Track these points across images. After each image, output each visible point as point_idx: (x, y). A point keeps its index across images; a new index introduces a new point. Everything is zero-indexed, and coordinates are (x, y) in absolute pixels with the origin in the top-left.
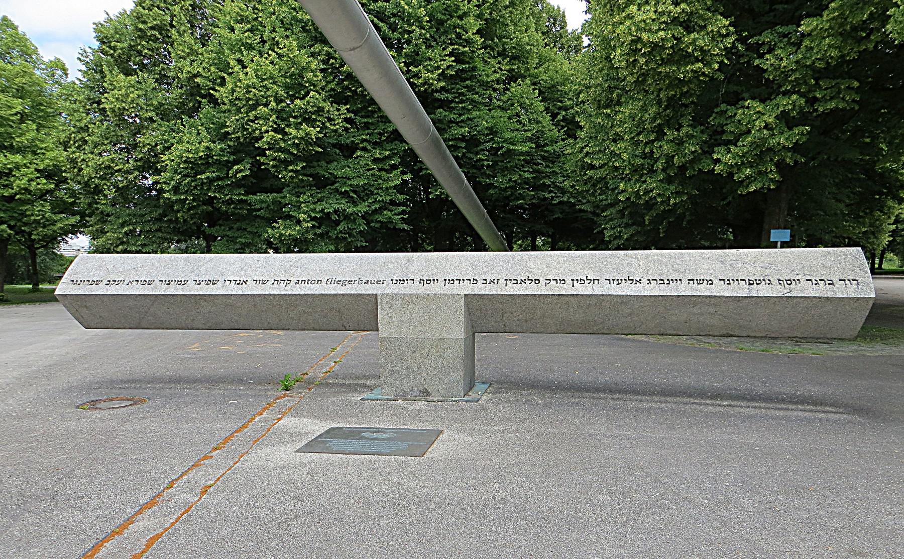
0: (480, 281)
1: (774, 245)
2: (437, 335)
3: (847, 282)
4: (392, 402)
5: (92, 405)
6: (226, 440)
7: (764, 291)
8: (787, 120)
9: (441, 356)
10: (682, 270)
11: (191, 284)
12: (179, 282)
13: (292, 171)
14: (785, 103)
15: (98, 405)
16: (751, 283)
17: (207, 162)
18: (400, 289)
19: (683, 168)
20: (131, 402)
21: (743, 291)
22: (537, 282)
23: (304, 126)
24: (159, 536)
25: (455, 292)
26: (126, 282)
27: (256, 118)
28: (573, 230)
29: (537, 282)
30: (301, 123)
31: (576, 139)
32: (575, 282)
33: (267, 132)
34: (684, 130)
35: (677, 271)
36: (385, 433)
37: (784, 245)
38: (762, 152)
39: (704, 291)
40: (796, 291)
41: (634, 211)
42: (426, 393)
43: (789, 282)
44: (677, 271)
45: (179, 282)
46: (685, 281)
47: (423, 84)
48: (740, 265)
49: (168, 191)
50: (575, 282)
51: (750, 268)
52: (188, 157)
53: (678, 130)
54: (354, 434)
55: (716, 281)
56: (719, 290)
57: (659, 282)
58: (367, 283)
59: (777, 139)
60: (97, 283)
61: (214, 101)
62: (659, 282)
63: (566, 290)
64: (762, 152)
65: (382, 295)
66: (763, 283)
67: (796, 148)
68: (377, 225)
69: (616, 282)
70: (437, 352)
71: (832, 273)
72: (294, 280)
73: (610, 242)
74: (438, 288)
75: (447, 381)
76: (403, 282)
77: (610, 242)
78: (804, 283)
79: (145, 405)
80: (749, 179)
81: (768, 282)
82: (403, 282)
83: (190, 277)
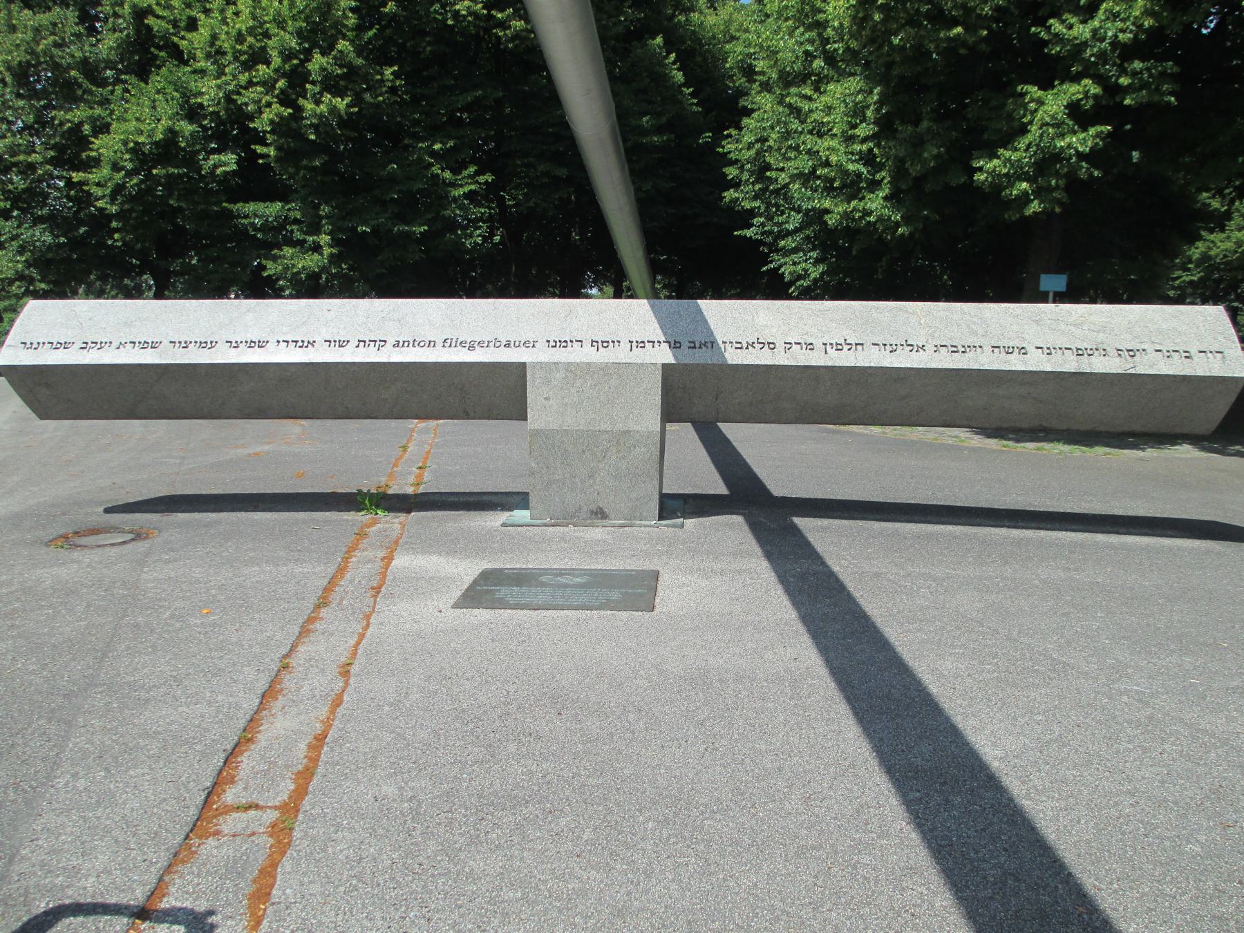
0: (685, 345)
1: (1042, 298)
2: (620, 426)
4: (551, 529)
5: (70, 540)
6: (329, 589)
7: (1099, 365)
8: (1079, 115)
9: (624, 457)
12: (203, 345)
13: (306, 168)
14: (1073, 91)
15: (83, 541)
17: (167, 149)
18: (561, 355)
19: (920, 180)
20: (131, 536)
21: (1070, 364)
22: (772, 346)
23: (327, 97)
24: (321, 739)
25: (648, 360)
26: (116, 344)
27: (250, 84)
29: (772, 346)
30: (321, 93)
31: (740, 129)
32: (828, 347)
33: (269, 105)
34: (925, 124)
35: (975, 333)
36: (574, 575)
37: (1060, 298)
38: (1047, 161)
39: (1015, 363)
41: (825, 238)
42: (600, 514)
43: (1132, 353)
44: (975, 333)
45: (203, 345)
46: (987, 349)
47: (513, 39)
48: (1063, 327)
49: (104, 197)
50: (828, 347)
51: (1078, 332)
52: (137, 143)
53: (916, 123)
54: (521, 578)
55: (1031, 349)
58: (508, 345)
59: (1068, 140)
61: (179, 56)
63: (816, 359)
64: (1047, 161)
67: (1091, 157)
69: (888, 347)
70: (619, 452)
71: (1173, 338)
72: (391, 341)
73: (791, 283)
74: (621, 354)
75: (634, 495)
76: (564, 344)
77: (791, 283)
79: (159, 540)
80: (1024, 199)
82: (564, 344)
83: (222, 336)
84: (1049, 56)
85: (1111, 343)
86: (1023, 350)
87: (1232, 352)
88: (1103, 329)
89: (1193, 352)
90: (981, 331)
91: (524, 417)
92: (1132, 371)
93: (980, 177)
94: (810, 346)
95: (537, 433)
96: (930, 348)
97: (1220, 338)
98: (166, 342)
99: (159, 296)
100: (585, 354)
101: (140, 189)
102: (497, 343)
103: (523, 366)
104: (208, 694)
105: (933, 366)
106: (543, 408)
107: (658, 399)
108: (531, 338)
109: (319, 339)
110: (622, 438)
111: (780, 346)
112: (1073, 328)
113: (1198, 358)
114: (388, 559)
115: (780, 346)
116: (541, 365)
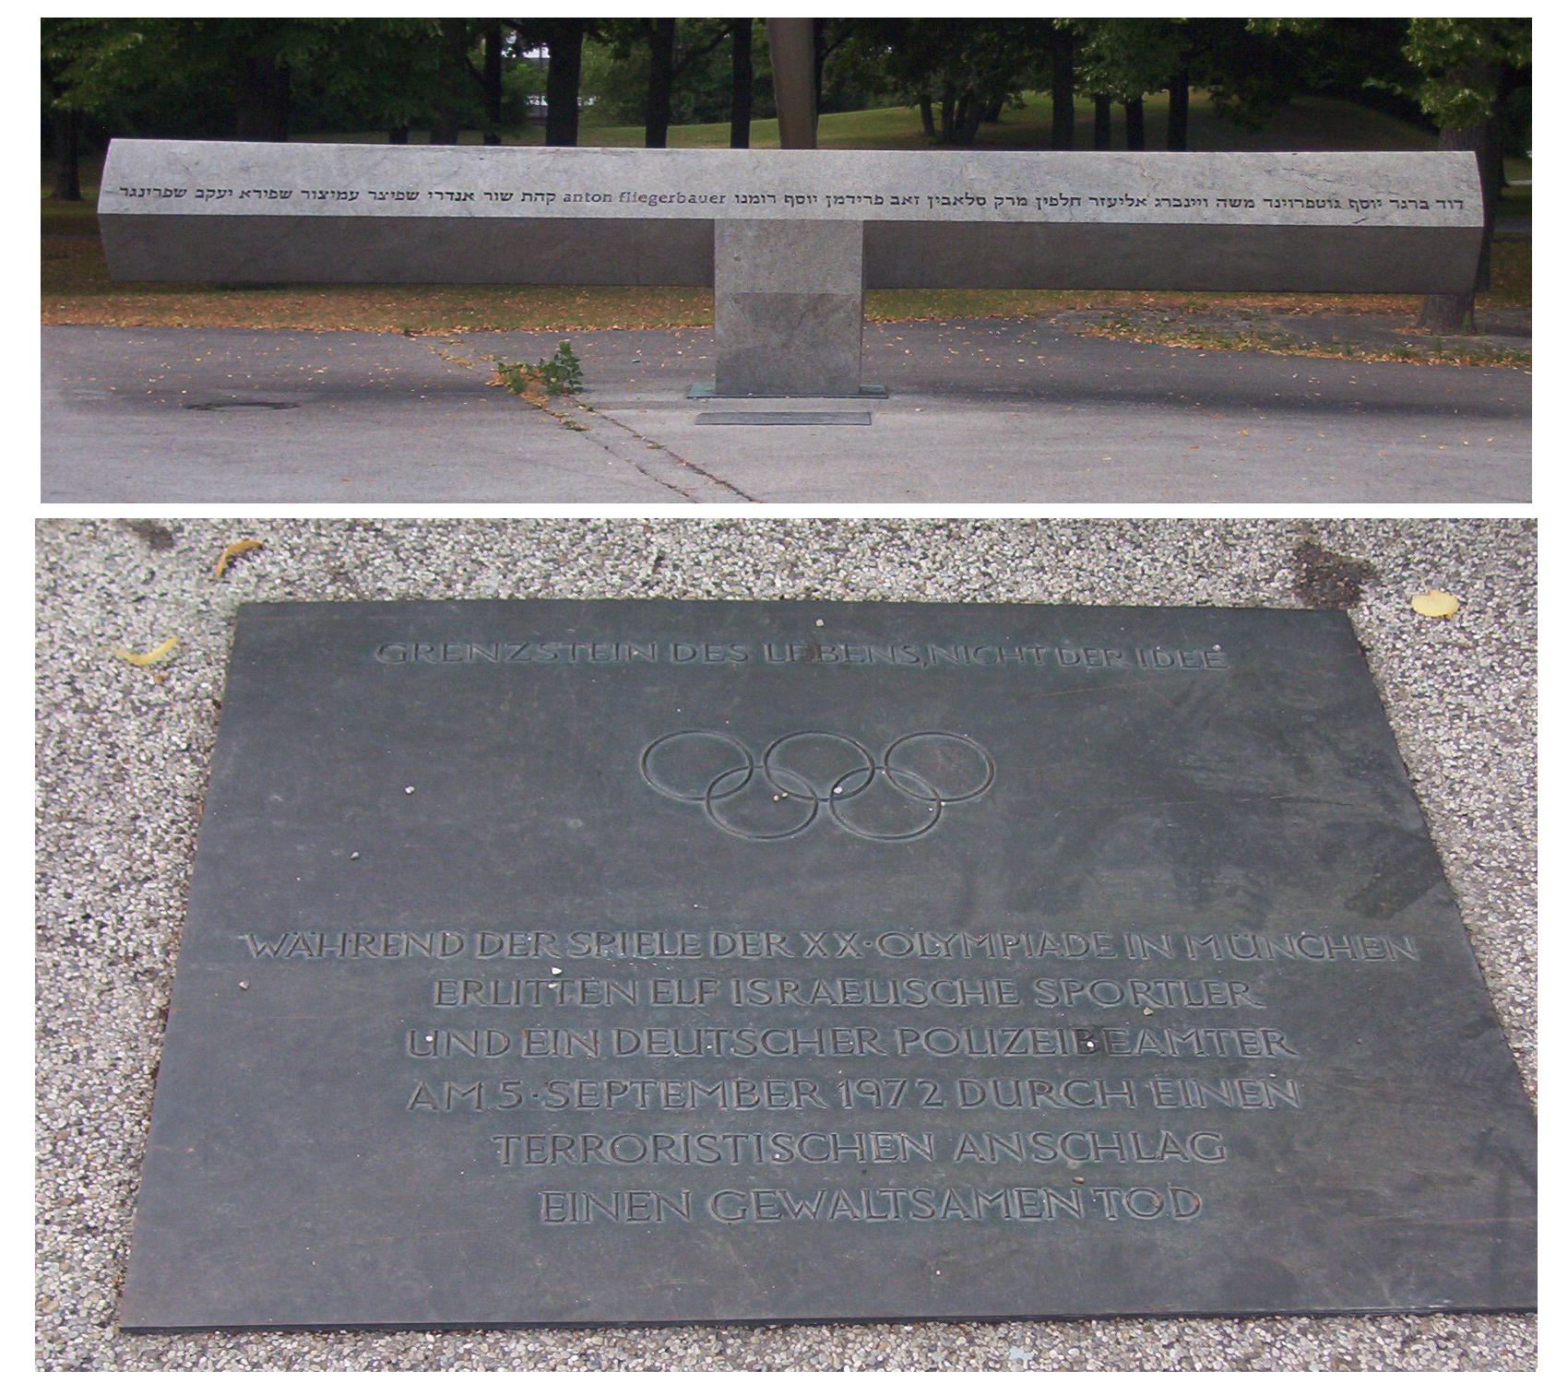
2: (818, 290)
22: (981, 201)
25: (848, 216)
29: (981, 201)
39: (1243, 217)
43: (1366, 204)
44: (1201, 186)
46: (1212, 203)
58: (692, 200)
63: (1030, 215)
76: (755, 199)
84: (1402, 59)
85: (1345, 191)
86: (1250, 203)
88: (1339, 179)
90: (1208, 183)
94: (1023, 201)
96: (1151, 202)
97: (1464, 187)
98: (296, 193)
100: (766, 212)
101: (1467, 43)
102: (681, 198)
105: (1154, 221)
106: (731, 272)
107: (859, 260)
108: (717, 191)
111: (991, 201)
115: (991, 201)
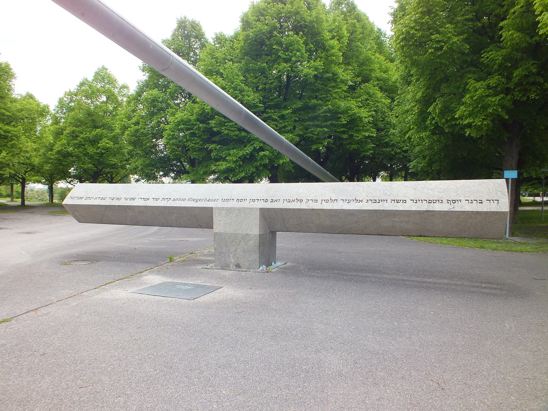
2: (245, 232)
3: (491, 201)
7: (437, 207)
10: (389, 193)
11: (123, 199)
14: (493, 81)
16: (430, 202)
21: (424, 207)
22: (301, 201)
25: (255, 206)
28: (349, 165)
29: (301, 201)
35: (386, 194)
39: (400, 207)
40: (457, 207)
43: (454, 201)
44: (386, 194)
56: (410, 206)
57: (479, 202)
60: (81, 198)
62: (479, 202)
65: (215, 208)
66: (438, 202)
68: (433, 50)
71: (489, 195)
72: (151, 198)
74: (245, 204)
75: (250, 259)
78: (463, 202)
81: (440, 201)
83: (123, 197)
87: (503, 200)
89: (484, 200)
91: (212, 227)
92: (452, 210)
93: (312, 150)
95: (216, 234)
99: (358, 181)
103: (212, 208)
104: (44, 360)
105: (364, 208)
109: (151, 198)
110: (245, 237)
112: (430, 191)
113: (485, 203)
114: (23, 187)
116: (218, 208)
